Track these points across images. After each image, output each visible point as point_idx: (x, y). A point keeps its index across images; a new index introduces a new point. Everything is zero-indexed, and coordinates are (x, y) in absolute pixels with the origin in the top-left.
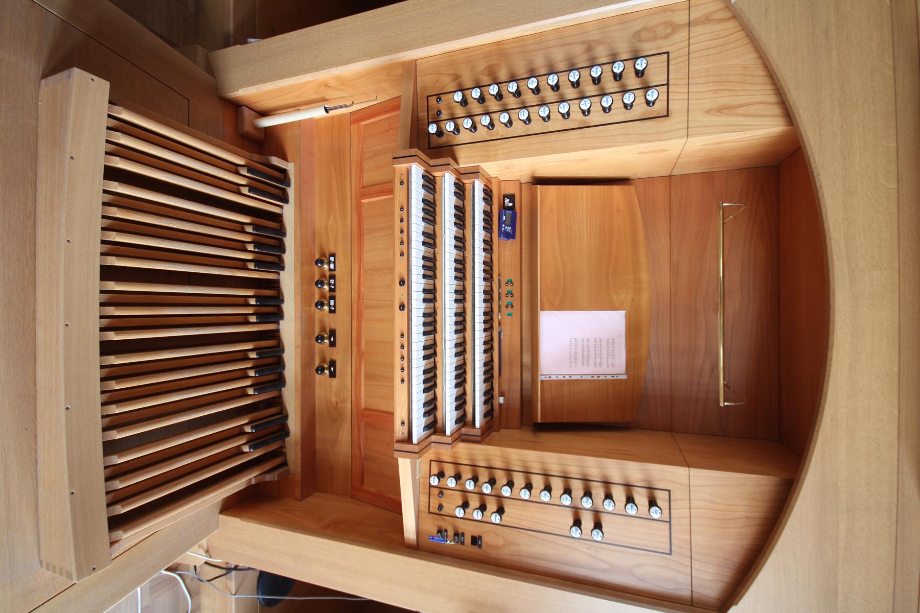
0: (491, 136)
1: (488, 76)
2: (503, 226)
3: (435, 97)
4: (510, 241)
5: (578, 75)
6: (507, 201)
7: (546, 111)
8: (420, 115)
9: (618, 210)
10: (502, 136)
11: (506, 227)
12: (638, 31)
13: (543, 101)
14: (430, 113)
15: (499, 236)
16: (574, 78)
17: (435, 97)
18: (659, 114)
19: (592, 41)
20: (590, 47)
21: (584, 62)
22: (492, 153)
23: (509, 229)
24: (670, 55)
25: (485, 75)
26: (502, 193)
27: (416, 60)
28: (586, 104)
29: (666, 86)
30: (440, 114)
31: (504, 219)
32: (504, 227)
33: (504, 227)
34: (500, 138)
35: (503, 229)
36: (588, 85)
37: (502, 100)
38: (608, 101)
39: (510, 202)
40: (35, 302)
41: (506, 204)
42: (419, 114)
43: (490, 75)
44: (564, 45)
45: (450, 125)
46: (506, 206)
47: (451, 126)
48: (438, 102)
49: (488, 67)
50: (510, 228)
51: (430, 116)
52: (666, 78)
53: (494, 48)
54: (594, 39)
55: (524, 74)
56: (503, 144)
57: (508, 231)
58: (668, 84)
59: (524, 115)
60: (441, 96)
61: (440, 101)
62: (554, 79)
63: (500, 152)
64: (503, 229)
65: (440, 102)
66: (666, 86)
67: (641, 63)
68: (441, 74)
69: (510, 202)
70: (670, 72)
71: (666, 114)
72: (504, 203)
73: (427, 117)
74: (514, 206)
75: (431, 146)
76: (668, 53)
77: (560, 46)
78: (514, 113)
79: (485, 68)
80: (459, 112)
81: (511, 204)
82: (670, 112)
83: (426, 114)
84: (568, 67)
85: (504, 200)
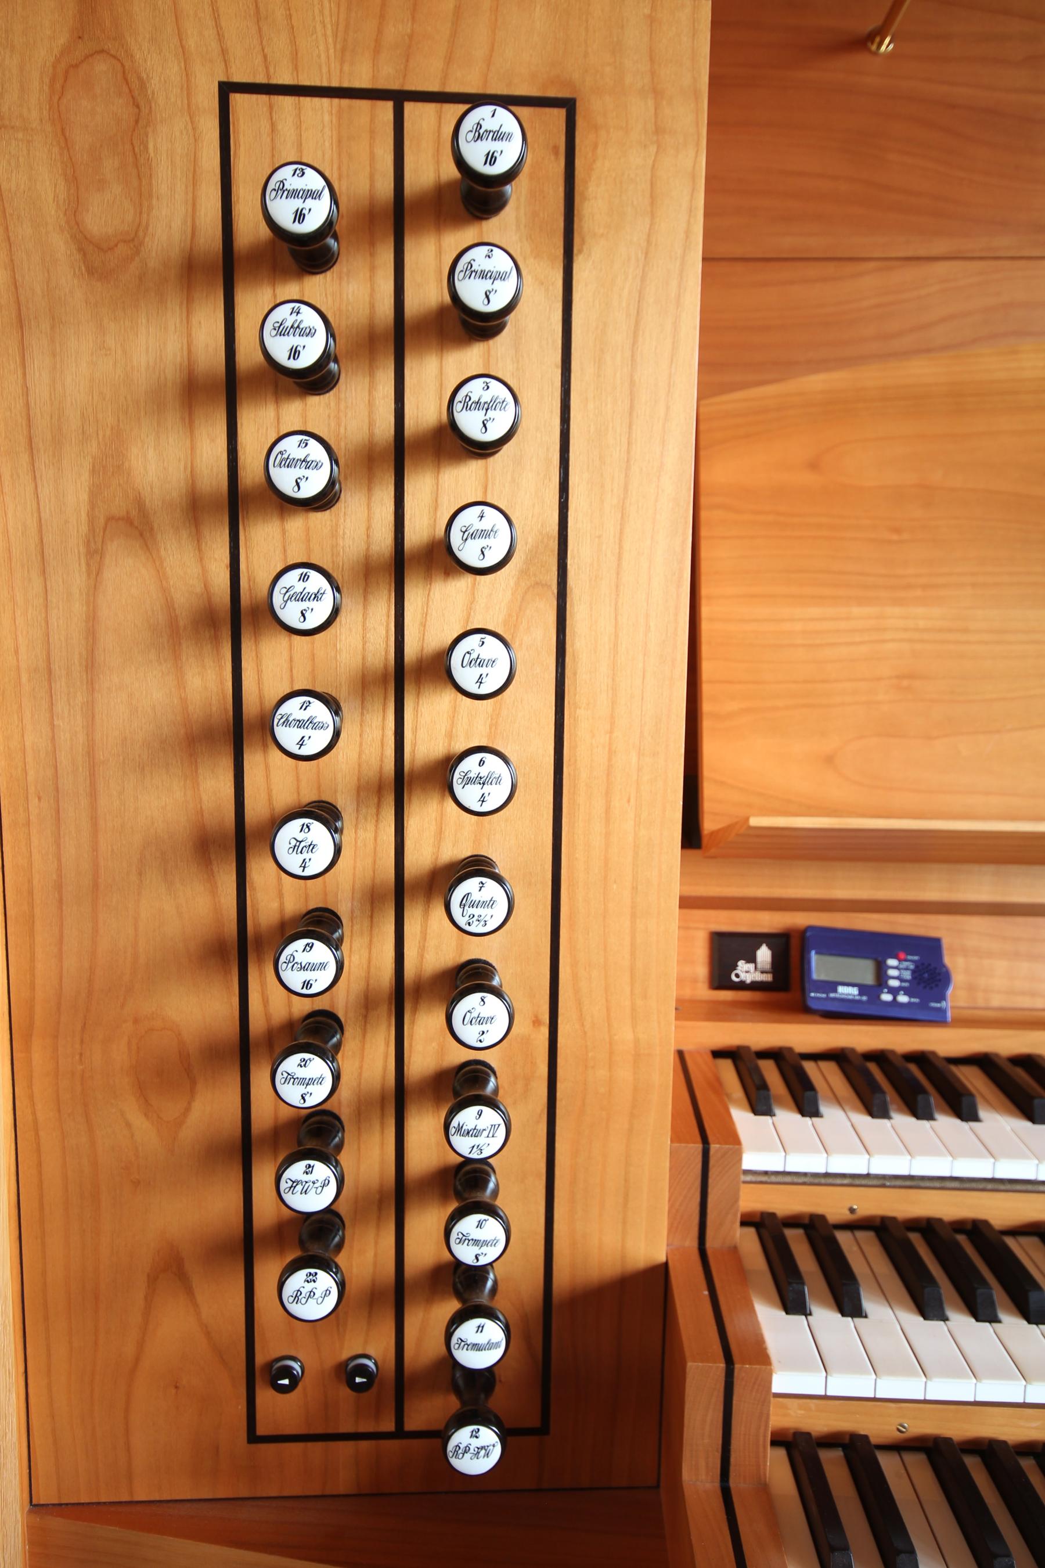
0: (528, 1080)
1: (192, 1092)
2: (887, 997)
3: (265, 1396)
4: (952, 961)
5: (304, 578)
6: (745, 972)
7: (484, 771)
8: (343, 1482)
9: (814, 465)
10: (536, 1022)
11: (894, 983)
12: (81, 250)
13: (379, 789)
14: (346, 1426)
15: (938, 1020)
16: (317, 596)
17: (265, 1396)
18: (555, 150)
19: (92, 505)
20: (128, 520)
21: (200, 550)
22: (624, 1074)
23: (897, 970)
24: (239, 77)
25: (188, 1110)
26: (703, 992)
27: (36, 1507)
28: (484, 534)
29: (409, 107)
30: (362, 1370)
31: (854, 991)
32: (894, 991)
33: (894, 991)
34: (545, 1031)
35: (903, 999)
36: (334, 534)
37: (341, 1015)
38: (486, 397)
39: (752, 959)
40: (9, 1209)
41: (759, 977)
42: (342, 1490)
43: (193, 1083)
44: (91, 665)
45: (477, 1347)
46: (768, 978)
47: (481, 1339)
48: (295, 1381)
49: (142, 1090)
50: (892, 962)
51: (364, 1427)
52: (364, 104)
53: (39, 1056)
54: (84, 497)
55: (214, 891)
56: (581, 1018)
57: (907, 975)
58: (399, 98)
59: (484, 904)
60: (260, 1359)
61: (287, 1372)
62: (304, 715)
63: (625, 1034)
64: (903, 999)
65: (296, 1366)
66: (409, 107)
67: (294, 194)
68: (137, 1360)
69: (752, 959)
70: (335, 84)
71: (559, 115)
72: (755, 986)
73: (364, 1444)
74: (772, 939)
75: (534, 1422)
76: (227, 89)
77: (91, 685)
78: (422, 949)
79: (147, 1108)
80: (370, 1255)
81: (764, 954)
82: (551, 93)
83: (346, 1448)
84: (216, 640)
85: (742, 986)
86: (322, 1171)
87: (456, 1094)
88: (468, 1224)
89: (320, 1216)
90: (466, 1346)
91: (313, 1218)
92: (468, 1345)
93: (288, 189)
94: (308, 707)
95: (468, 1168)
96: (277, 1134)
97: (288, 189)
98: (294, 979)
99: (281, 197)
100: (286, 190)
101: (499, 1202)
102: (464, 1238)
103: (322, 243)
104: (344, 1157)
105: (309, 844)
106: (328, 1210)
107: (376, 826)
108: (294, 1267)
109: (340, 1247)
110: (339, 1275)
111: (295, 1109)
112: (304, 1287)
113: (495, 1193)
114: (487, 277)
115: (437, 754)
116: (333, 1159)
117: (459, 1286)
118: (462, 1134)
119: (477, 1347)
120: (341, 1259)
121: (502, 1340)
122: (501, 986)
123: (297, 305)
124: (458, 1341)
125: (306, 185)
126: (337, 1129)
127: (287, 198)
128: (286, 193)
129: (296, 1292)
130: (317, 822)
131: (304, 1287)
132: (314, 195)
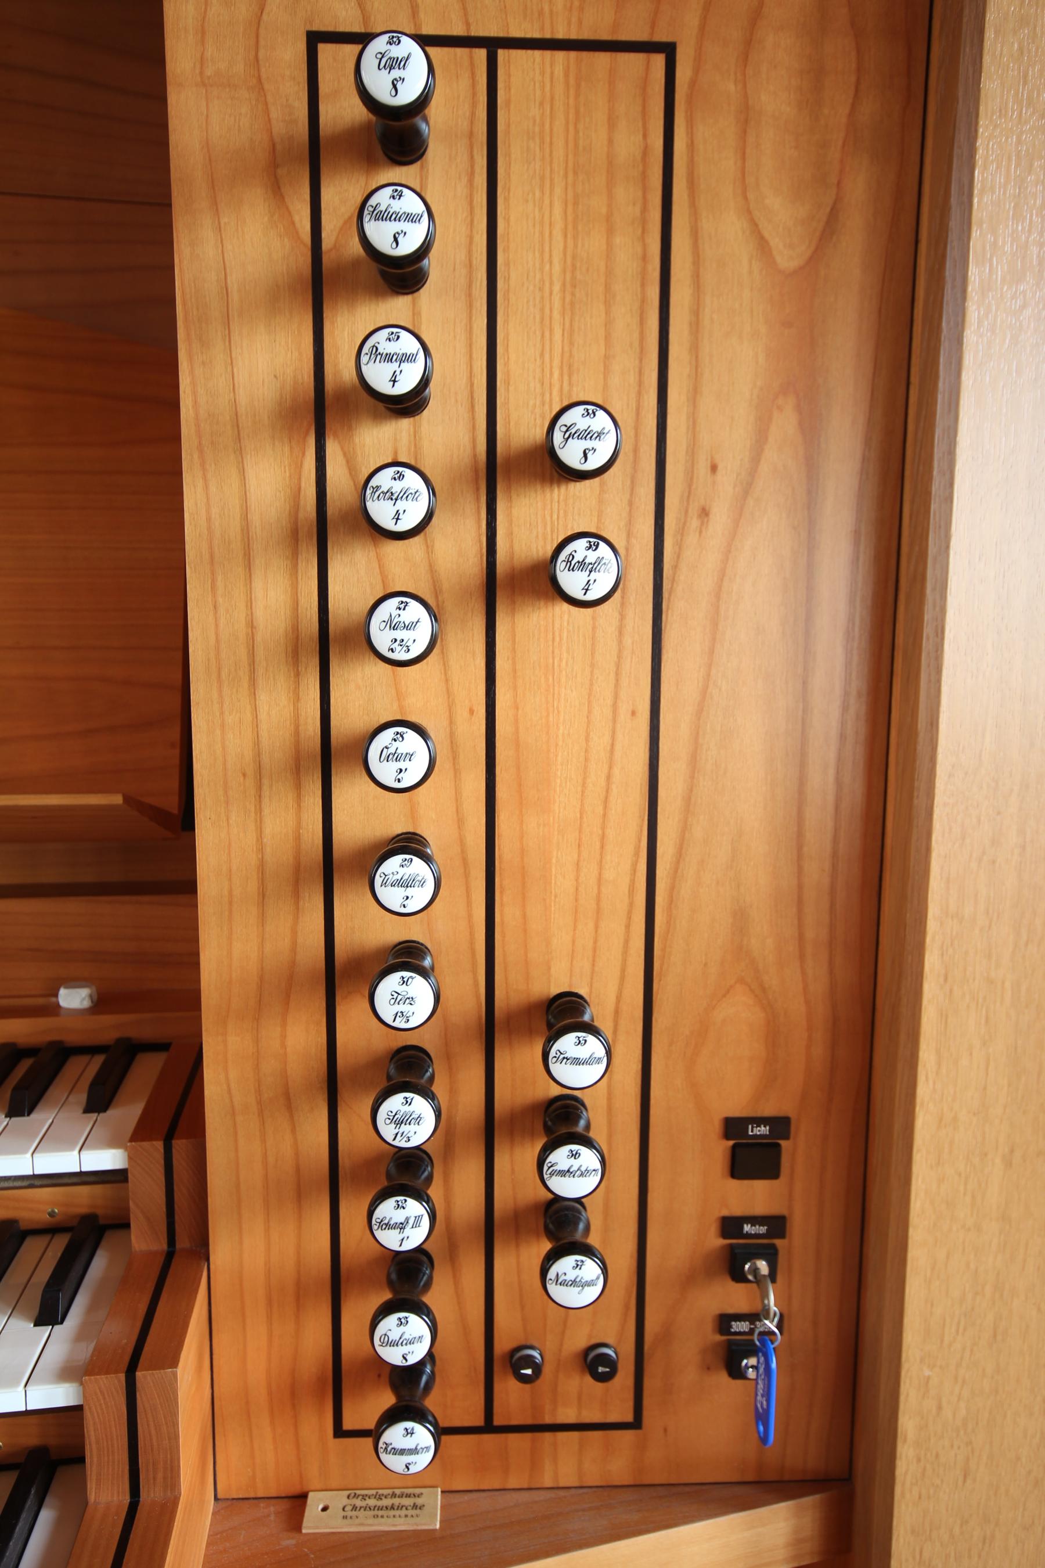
29: (502, 54)
45: (577, 1061)
66: (502, 54)
86: (414, 1208)
87: (548, 1130)
88: (560, 1157)
89: (407, 1254)
90: (565, 1060)
91: (402, 1255)
92: (568, 1059)
93: (381, 353)
94: (407, 607)
95: (556, 1206)
96: (368, 1166)
97: (381, 353)
98: (392, 897)
99: (375, 362)
100: (380, 354)
101: (592, 1134)
102: (562, 1056)
103: (416, 266)
104: (435, 1191)
105: (416, 491)
106: (419, 1250)
107: (455, 1276)
108: (386, 1310)
109: (428, 1285)
110: (436, 1102)
111: (384, 1249)
112: (390, 1330)
113: (588, 1127)
114: (575, 437)
115: (535, 553)
116: (425, 1195)
117: (551, 1226)
118: (571, 568)
119: (577, 1061)
120: (430, 1403)
121: (598, 1278)
122: (593, 1020)
123: (395, 330)
124: (556, 1054)
125: (400, 349)
126: (426, 1163)
127: (380, 362)
128: (379, 357)
129: (383, 1337)
130: (415, 602)
131: (390, 1330)
132: (411, 218)
